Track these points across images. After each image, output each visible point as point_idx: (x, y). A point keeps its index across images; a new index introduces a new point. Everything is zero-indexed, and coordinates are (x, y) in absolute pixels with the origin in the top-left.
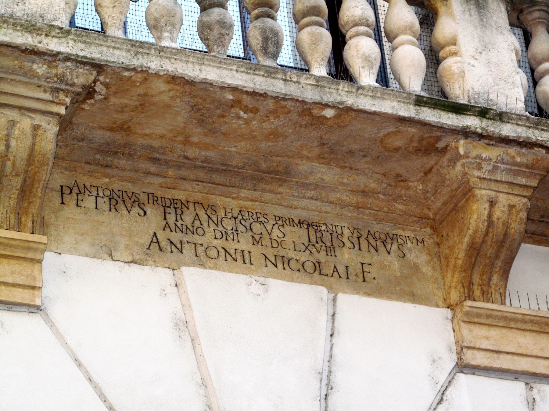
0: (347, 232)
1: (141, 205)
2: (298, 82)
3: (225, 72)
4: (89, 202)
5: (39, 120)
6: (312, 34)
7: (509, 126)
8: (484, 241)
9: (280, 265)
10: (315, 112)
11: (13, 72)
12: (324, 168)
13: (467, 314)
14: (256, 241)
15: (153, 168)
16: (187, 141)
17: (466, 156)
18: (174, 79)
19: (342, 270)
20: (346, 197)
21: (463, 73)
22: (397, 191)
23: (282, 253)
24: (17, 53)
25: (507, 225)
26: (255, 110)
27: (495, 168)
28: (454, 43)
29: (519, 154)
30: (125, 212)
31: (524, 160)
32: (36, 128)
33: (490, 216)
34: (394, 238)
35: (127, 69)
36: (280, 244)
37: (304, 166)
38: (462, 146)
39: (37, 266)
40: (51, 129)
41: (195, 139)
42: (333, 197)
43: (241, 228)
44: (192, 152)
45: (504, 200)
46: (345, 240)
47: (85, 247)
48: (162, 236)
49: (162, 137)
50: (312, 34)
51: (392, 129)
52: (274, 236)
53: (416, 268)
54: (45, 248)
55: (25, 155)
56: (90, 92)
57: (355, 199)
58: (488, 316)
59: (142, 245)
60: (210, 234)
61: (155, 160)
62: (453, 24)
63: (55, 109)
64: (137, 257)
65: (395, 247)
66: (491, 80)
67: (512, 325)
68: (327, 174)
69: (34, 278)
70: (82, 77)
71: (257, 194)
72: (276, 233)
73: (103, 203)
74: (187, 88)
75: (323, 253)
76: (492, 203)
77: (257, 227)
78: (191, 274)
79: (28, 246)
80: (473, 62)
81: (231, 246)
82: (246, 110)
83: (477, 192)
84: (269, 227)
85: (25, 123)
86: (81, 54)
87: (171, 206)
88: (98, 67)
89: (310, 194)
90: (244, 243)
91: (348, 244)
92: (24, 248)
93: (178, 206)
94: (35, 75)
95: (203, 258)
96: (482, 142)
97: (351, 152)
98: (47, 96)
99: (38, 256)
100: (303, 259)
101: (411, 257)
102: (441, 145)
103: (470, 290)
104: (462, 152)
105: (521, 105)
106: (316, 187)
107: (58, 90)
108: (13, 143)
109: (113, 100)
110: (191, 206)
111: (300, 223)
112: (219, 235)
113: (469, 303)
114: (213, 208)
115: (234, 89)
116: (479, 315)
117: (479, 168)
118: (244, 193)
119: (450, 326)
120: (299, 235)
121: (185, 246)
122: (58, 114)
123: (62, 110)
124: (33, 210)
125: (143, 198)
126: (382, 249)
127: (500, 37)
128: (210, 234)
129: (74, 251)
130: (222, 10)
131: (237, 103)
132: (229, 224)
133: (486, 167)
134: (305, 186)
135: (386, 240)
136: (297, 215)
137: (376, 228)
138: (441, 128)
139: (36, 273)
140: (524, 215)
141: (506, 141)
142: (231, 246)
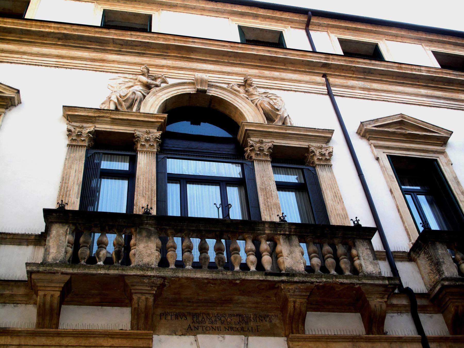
0: (252, 316)
1: (185, 316)
2: (226, 274)
3: (203, 274)
4: (169, 318)
5: (147, 296)
6: (234, 257)
7: (297, 278)
8: (294, 314)
9: (230, 330)
10: (234, 282)
11: (138, 283)
12: (243, 297)
13: (291, 338)
14: (222, 323)
15: (189, 304)
16: (198, 295)
17: (284, 289)
18: (187, 278)
19: (250, 328)
20: (251, 305)
21: (284, 262)
22: (268, 301)
23: (231, 326)
24: (139, 277)
25: (300, 308)
26: (215, 284)
27: (294, 291)
28: (282, 253)
29: (301, 286)
30: (180, 319)
31: (303, 287)
32: (147, 298)
33: (294, 306)
34: (268, 316)
35: (172, 277)
36: (230, 323)
37: (236, 297)
38: (282, 286)
39: (151, 341)
40: (151, 299)
41: (201, 294)
42: (247, 306)
43: (217, 320)
44: (200, 298)
45: (298, 300)
46: (252, 319)
47: (167, 332)
48: (191, 325)
49: (191, 294)
50: (234, 257)
51: (259, 284)
52: (228, 321)
53: (275, 324)
54: (153, 334)
55: (144, 307)
56: (163, 285)
57: (254, 305)
58: (298, 338)
59: (185, 329)
60: (207, 322)
61: (189, 302)
62: (281, 247)
63: (152, 292)
64: (184, 333)
65: (268, 319)
66: (293, 263)
67: (306, 340)
68: (244, 299)
69: (150, 344)
70: (159, 282)
71: (222, 308)
72: (229, 320)
73: (173, 317)
74: (192, 280)
75: (244, 324)
76: (295, 302)
77: (223, 319)
78: (200, 337)
79: (147, 335)
80: (287, 258)
81: (214, 326)
82: (212, 284)
83: (289, 299)
84: (227, 318)
85: (143, 298)
86: (158, 275)
87: (194, 315)
88: (164, 278)
89: (240, 306)
90: (218, 325)
91: (253, 320)
92: (146, 335)
93: (198, 315)
94: (145, 283)
95: (205, 331)
96: (289, 284)
97: (250, 292)
98: (150, 288)
99: (151, 337)
100: (237, 327)
101: (273, 322)
102: (276, 286)
103: (292, 330)
104: (282, 288)
105: (303, 269)
106: (241, 303)
107: (153, 286)
108: (140, 304)
109: (172, 286)
110: (201, 315)
111: (237, 315)
112: (210, 323)
113: (291, 335)
114: (208, 314)
115: (207, 279)
116: (295, 338)
117: (289, 292)
118: (218, 308)
119: (286, 343)
120: (236, 319)
121: (199, 327)
122: (153, 293)
123: (154, 292)
124: (149, 323)
125: (186, 314)
126: (264, 321)
127: (296, 248)
128: (207, 322)
129: (164, 334)
130: (205, 254)
131: (209, 283)
132: (213, 319)
133: (291, 291)
134: (238, 303)
135: (266, 317)
136: (235, 313)
137: (262, 313)
138: (274, 281)
139: (150, 342)
140: (305, 305)
141: (296, 282)
142: (214, 326)
